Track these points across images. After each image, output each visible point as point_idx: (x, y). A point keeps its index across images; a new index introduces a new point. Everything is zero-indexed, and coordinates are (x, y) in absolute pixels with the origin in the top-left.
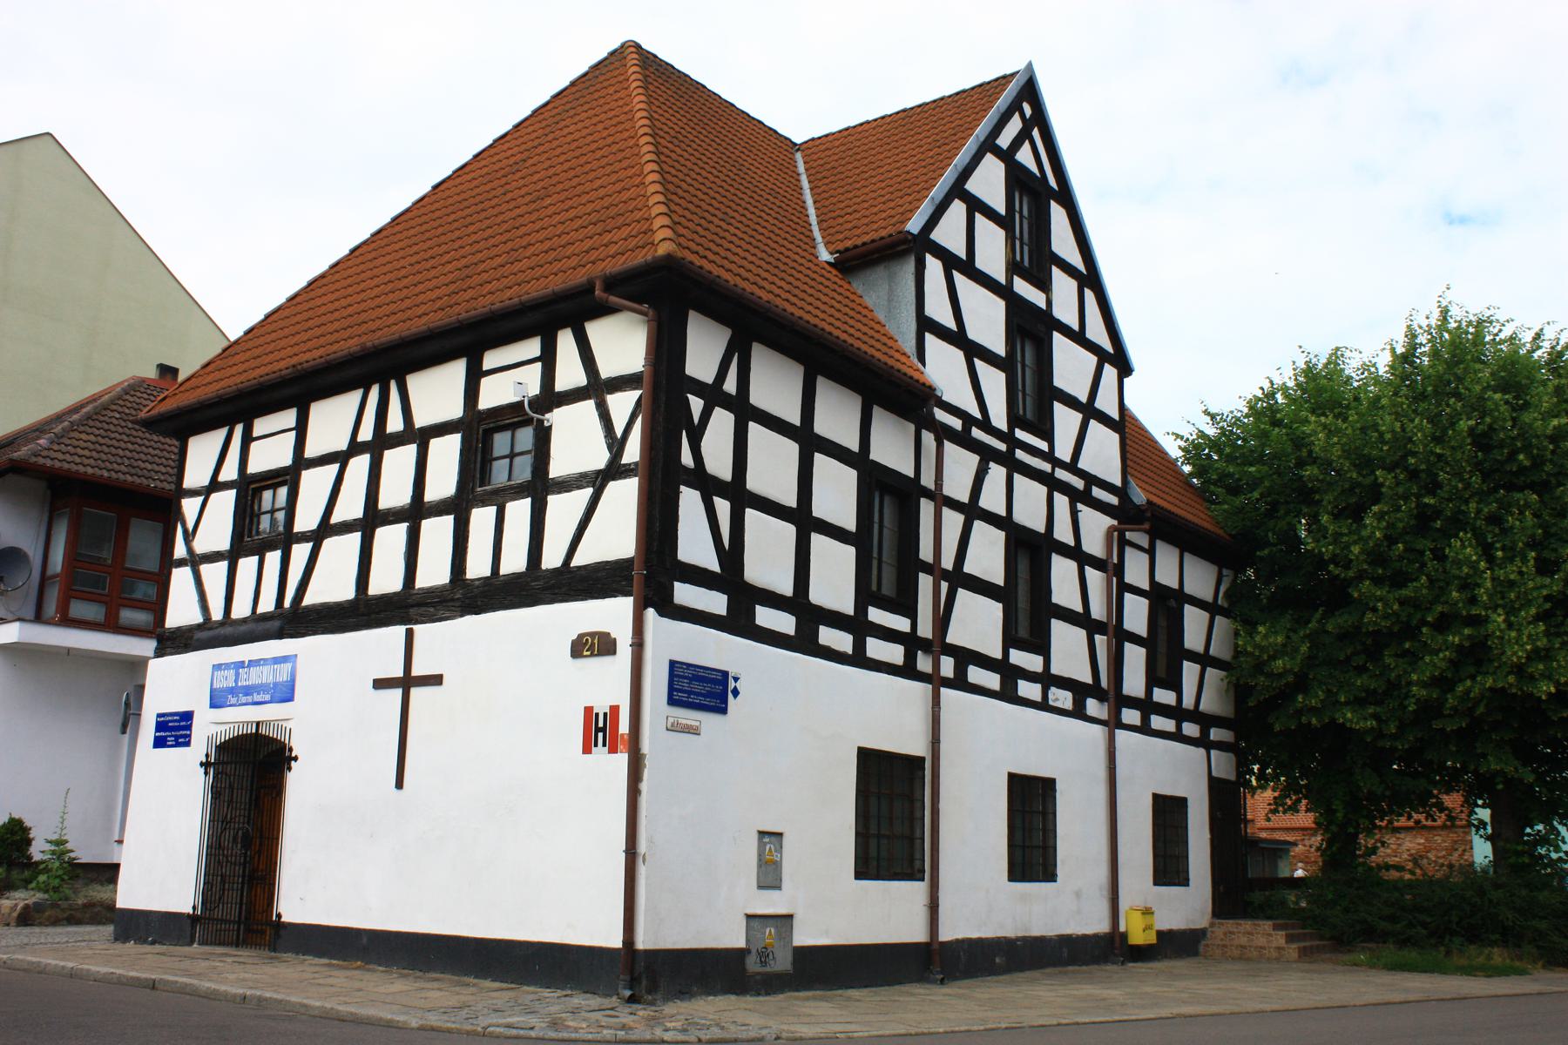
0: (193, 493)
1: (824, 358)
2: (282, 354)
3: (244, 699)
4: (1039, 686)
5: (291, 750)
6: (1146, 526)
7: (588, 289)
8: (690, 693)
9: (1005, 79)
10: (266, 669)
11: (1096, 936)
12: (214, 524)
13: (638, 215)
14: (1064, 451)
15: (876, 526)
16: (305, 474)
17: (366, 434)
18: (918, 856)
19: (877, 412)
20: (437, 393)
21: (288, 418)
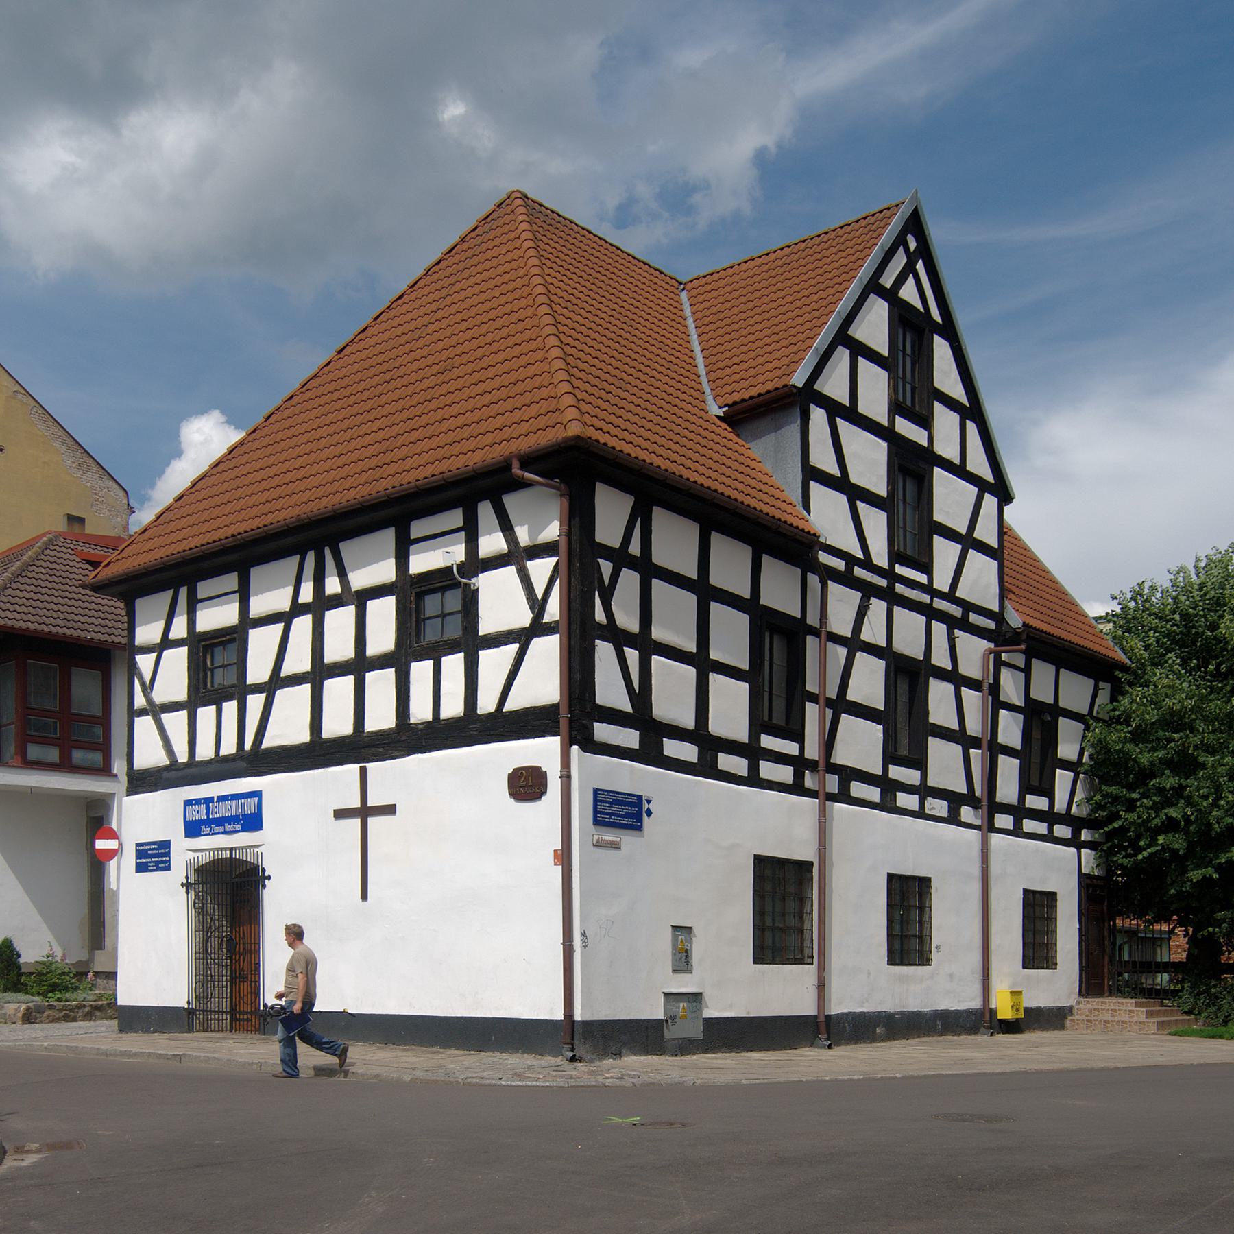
0: (146, 650)
1: (715, 515)
2: (218, 522)
3: (217, 829)
4: (916, 797)
5: (264, 870)
6: (1023, 647)
7: (505, 467)
9: (888, 211)
10: (234, 803)
11: (968, 1012)
12: (172, 676)
13: (545, 393)
14: (942, 582)
15: (767, 663)
17: (307, 594)
18: (807, 943)
19: (766, 559)
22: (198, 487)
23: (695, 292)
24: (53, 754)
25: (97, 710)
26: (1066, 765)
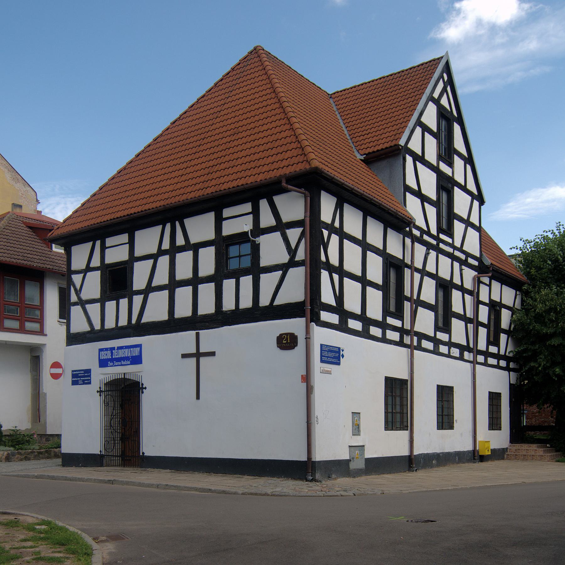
0: (77, 272)
1: (371, 209)
3: (117, 364)
5: (142, 384)
6: (490, 275)
8: (328, 357)
10: (126, 350)
16: (136, 264)
17: (166, 245)
19: (389, 230)
20: (201, 228)
21: (124, 238)
22: (103, 190)
23: (337, 99)
24: (15, 324)
25: (37, 302)
26: (504, 331)
